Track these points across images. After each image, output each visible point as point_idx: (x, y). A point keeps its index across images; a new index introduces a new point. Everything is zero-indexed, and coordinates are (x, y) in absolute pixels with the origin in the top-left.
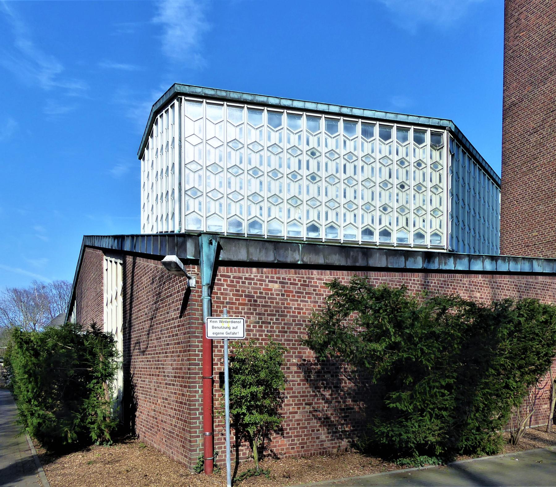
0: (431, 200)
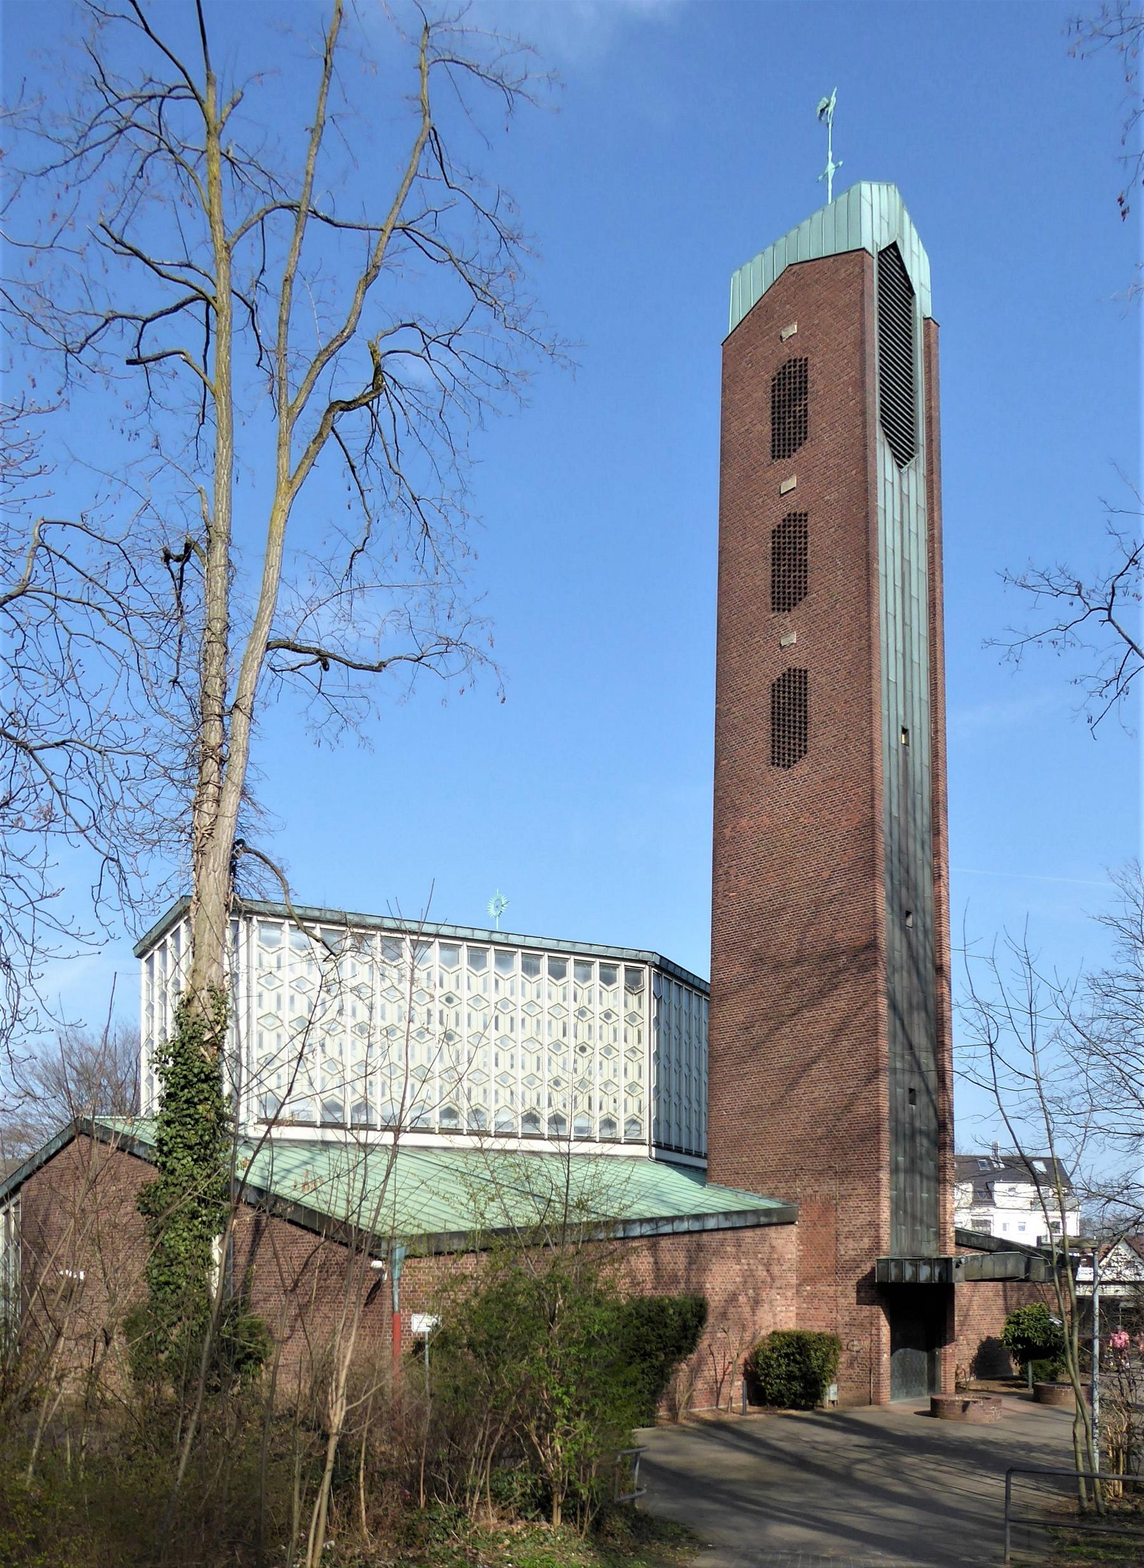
0: (626, 1070)
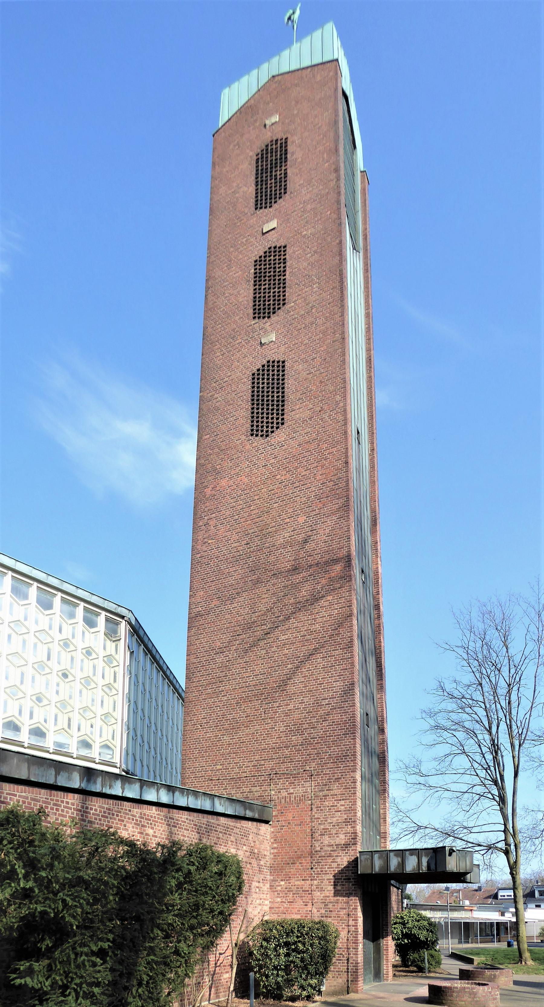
0: (102, 702)
